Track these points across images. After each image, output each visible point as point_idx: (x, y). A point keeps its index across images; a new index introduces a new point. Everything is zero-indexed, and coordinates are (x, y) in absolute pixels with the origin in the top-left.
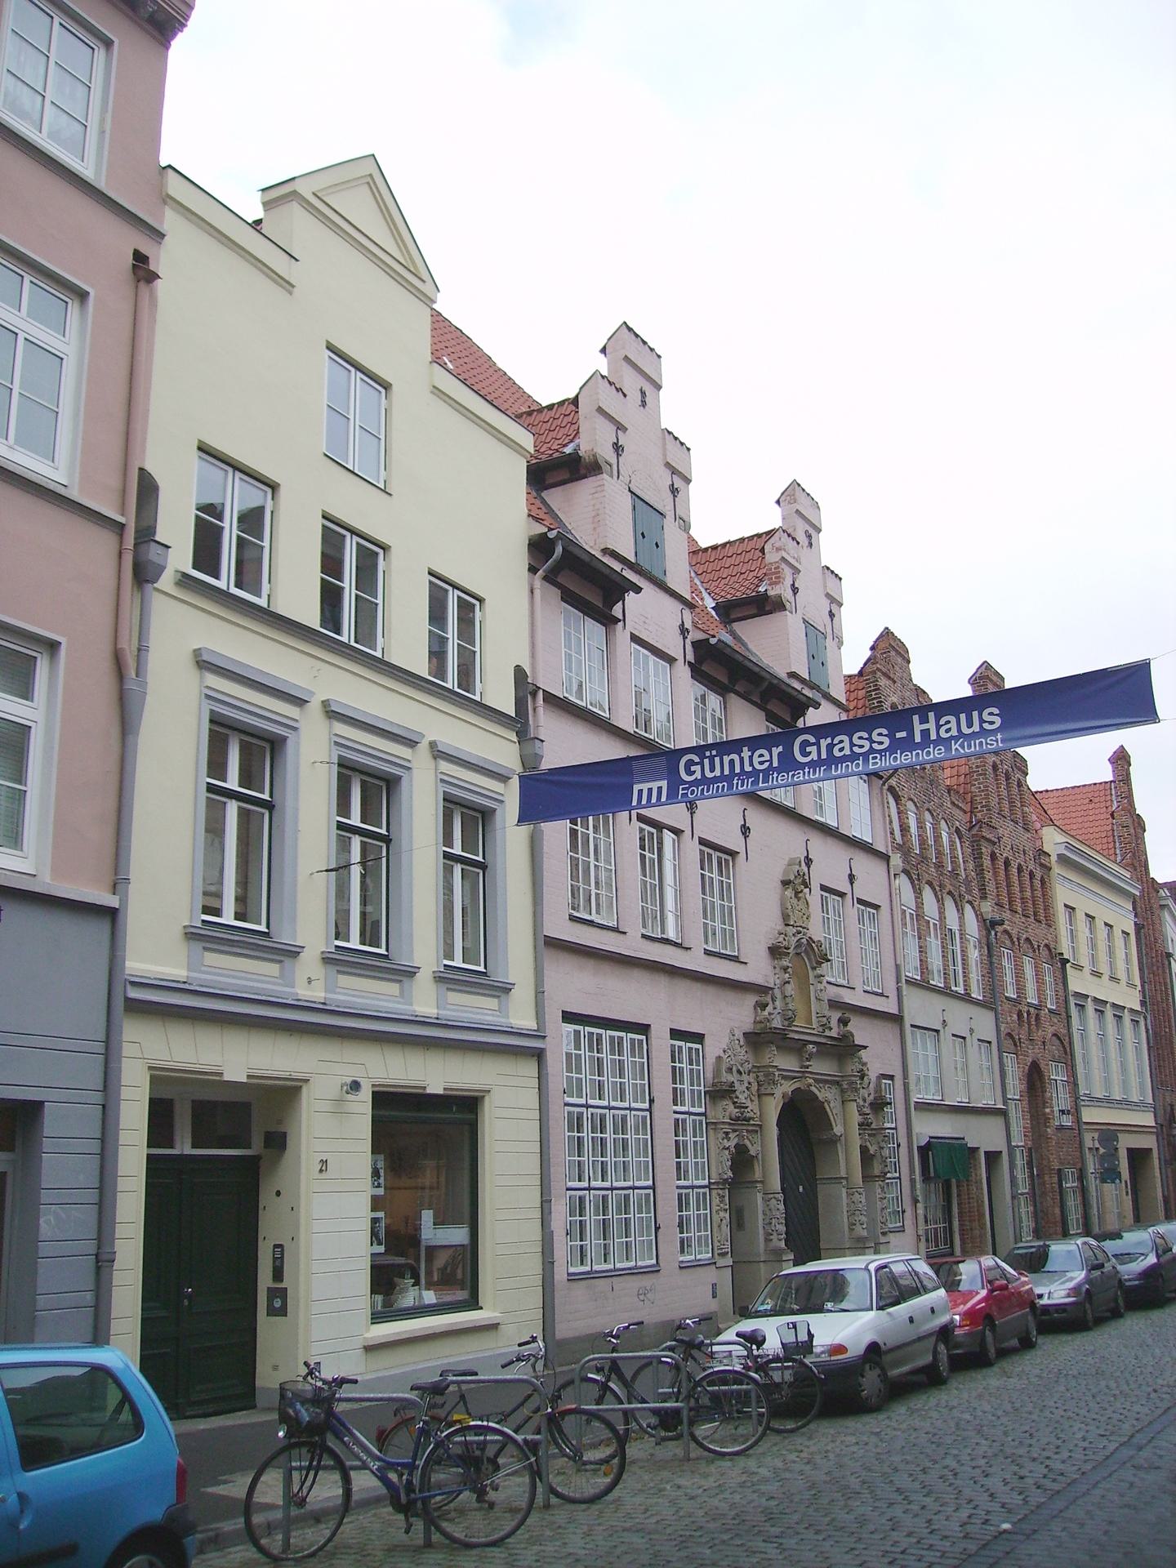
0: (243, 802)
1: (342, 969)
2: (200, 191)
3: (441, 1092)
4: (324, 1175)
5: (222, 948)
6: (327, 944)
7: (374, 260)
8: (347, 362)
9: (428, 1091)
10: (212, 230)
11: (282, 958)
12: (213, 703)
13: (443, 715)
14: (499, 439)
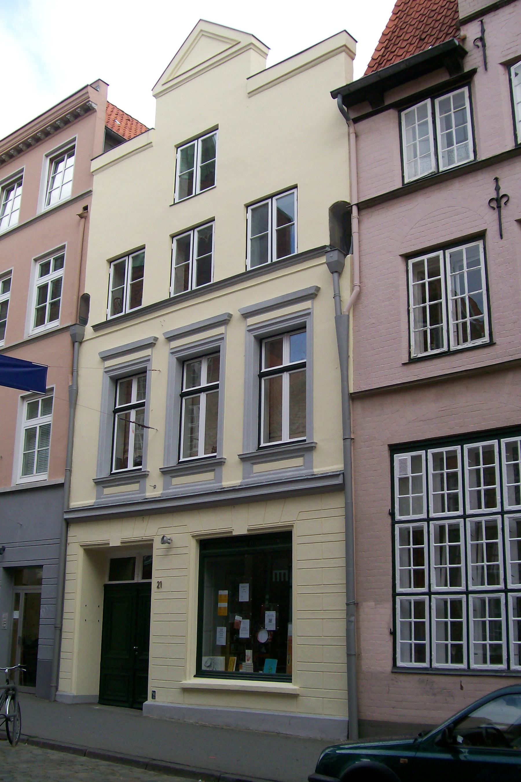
0: (207, 391)
1: (173, 475)
2: (325, 42)
3: (118, 544)
4: (160, 590)
5: (268, 459)
6: (164, 465)
7: (206, 70)
8: (188, 143)
9: (234, 533)
10: (116, 162)
11: (303, 453)
12: (176, 354)
13: (256, 287)
14: (313, 66)
